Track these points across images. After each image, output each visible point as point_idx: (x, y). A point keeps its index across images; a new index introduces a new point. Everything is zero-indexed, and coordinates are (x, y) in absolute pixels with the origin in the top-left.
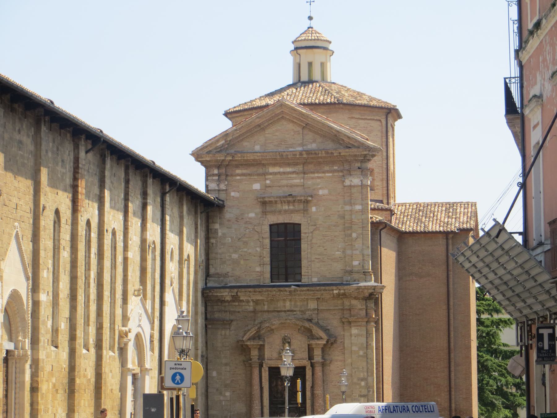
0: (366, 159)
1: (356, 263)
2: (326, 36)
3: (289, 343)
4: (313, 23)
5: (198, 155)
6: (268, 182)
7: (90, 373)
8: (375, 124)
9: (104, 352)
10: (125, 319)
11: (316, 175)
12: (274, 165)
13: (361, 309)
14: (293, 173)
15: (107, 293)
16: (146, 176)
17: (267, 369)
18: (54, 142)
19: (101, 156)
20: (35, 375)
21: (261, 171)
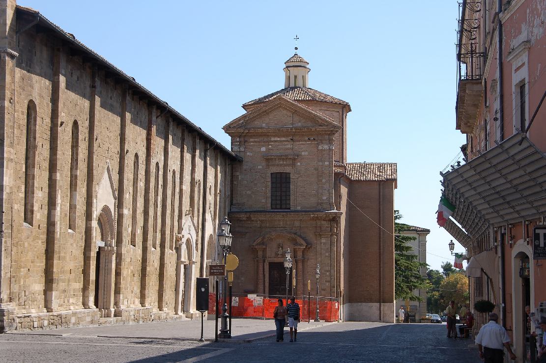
0: (332, 133)
1: (325, 198)
2: (306, 60)
3: (282, 247)
4: (298, 52)
5: (228, 129)
6: (270, 147)
7: (157, 264)
8: (336, 114)
9: (166, 250)
10: (180, 229)
11: (301, 143)
12: (274, 136)
13: (328, 227)
14: (286, 141)
15: (168, 212)
16: (195, 138)
17: (268, 264)
18: (135, 108)
19: (167, 121)
20: (118, 264)
21: (266, 139)
